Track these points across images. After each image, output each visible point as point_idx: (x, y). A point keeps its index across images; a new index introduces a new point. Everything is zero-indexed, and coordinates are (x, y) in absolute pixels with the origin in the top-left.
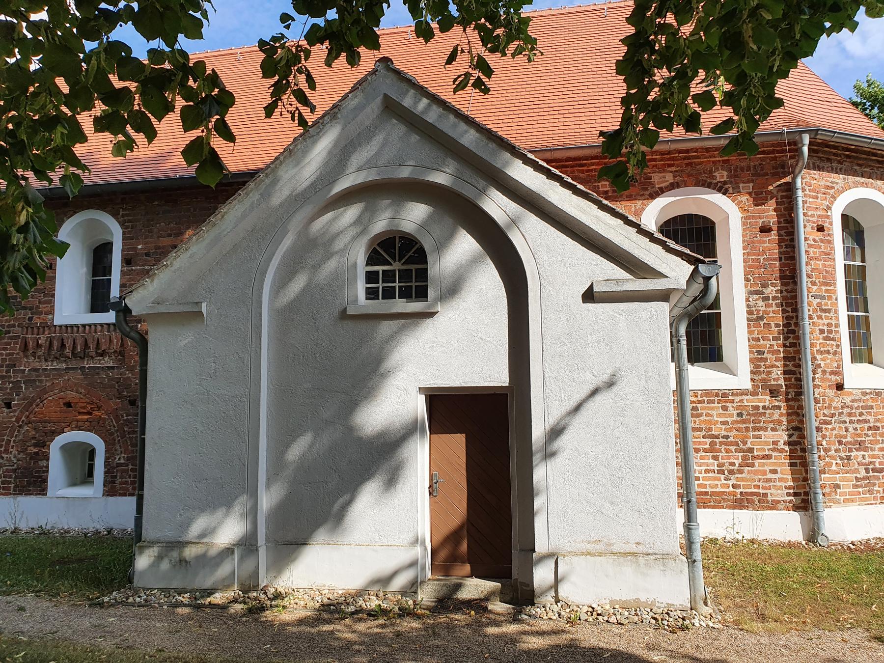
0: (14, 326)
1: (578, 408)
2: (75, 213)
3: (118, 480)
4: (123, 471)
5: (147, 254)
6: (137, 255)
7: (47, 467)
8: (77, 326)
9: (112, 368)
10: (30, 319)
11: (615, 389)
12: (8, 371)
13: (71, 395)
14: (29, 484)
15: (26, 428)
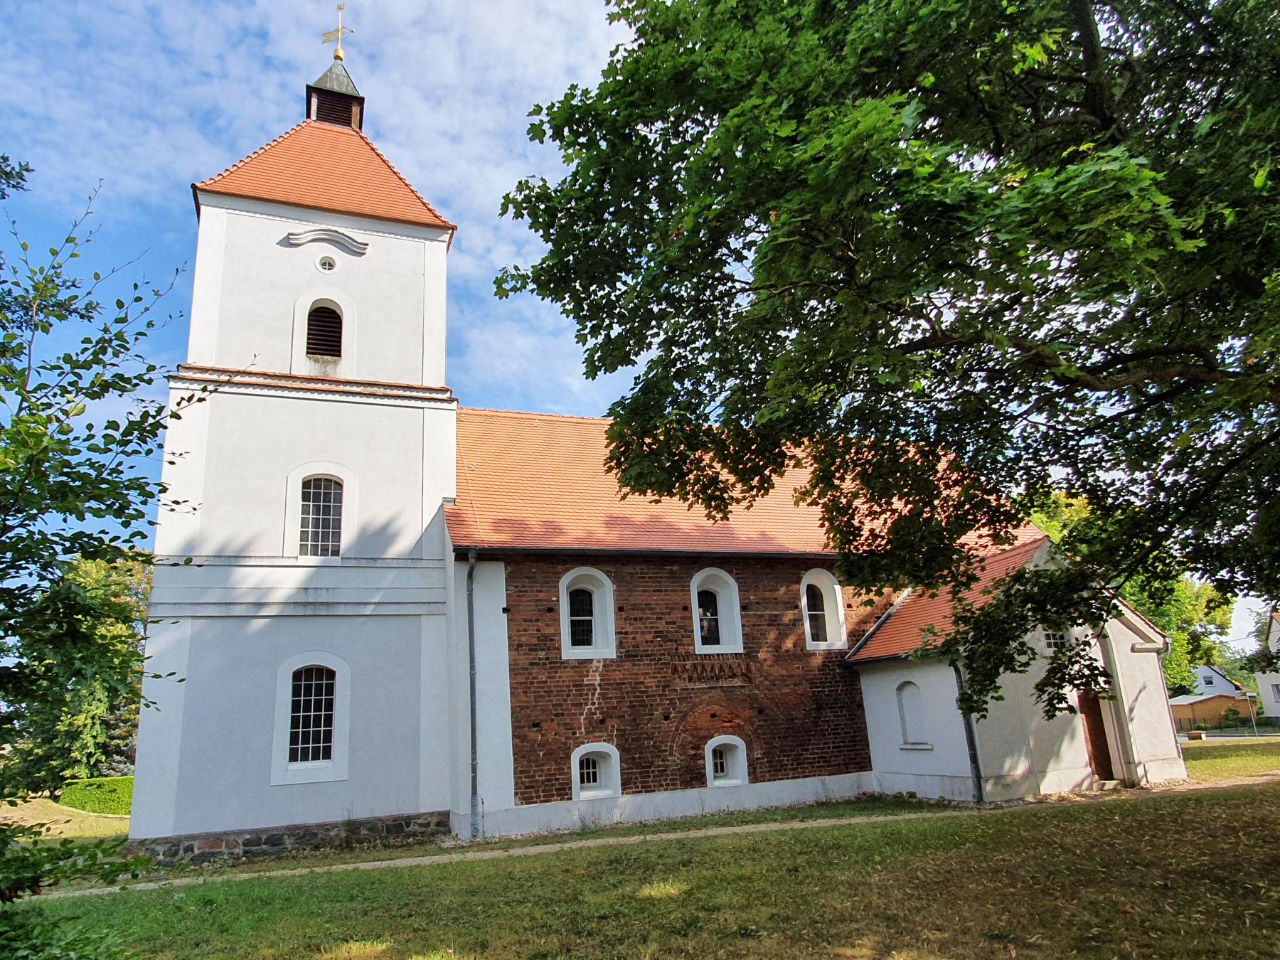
0: (664, 654)
1: (1136, 699)
2: (701, 569)
3: (758, 771)
4: (761, 763)
5: (758, 603)
6: (751, 603)
7: (704, 765)
8: (713, 655)
9: (741, 687)
10: (677, 649)
11: (1000, 702)
12: (664, 690)
13: (715, 708)
14: (692, 779)
15: (683, 735)
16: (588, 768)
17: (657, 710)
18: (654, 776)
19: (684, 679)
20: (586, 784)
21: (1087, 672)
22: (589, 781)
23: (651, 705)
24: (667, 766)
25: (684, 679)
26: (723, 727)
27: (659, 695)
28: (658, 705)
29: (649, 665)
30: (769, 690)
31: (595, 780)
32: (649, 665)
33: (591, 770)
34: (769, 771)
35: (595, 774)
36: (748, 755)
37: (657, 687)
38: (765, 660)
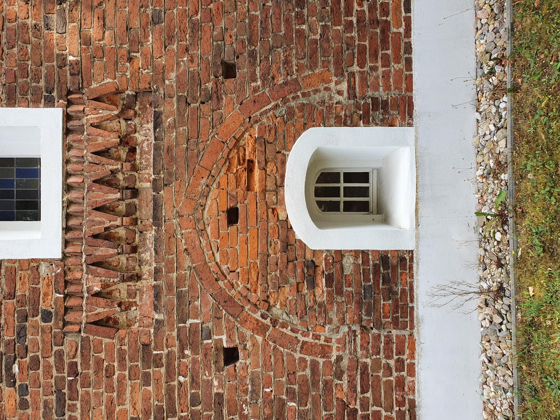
0: (60, 355)
1: (228, 179)
3: (382, 94)
7: (356, 253)
10: (47, 316)
14: (390, 293)
15: (277, 310)
16: (335, 192)
17: (209, 384)
18: (377, 403)
19: (131, 294)
20: (372, 199)
21: (35, 53)
22: (365, 192)
23: (195, 401)
24: (355, 363)
25: (131, 294)
26: (264, 191)
27: (170, 375)
28: (194, 382)
29: (86, 402)
30: (170, 38)
31: (364, 177)
32: (86, 402)
33: (342, 199)
34: (386, 62)
35: (350, 177)
36: (342, 122)
37: (147, 383)
38: (86, 41)
